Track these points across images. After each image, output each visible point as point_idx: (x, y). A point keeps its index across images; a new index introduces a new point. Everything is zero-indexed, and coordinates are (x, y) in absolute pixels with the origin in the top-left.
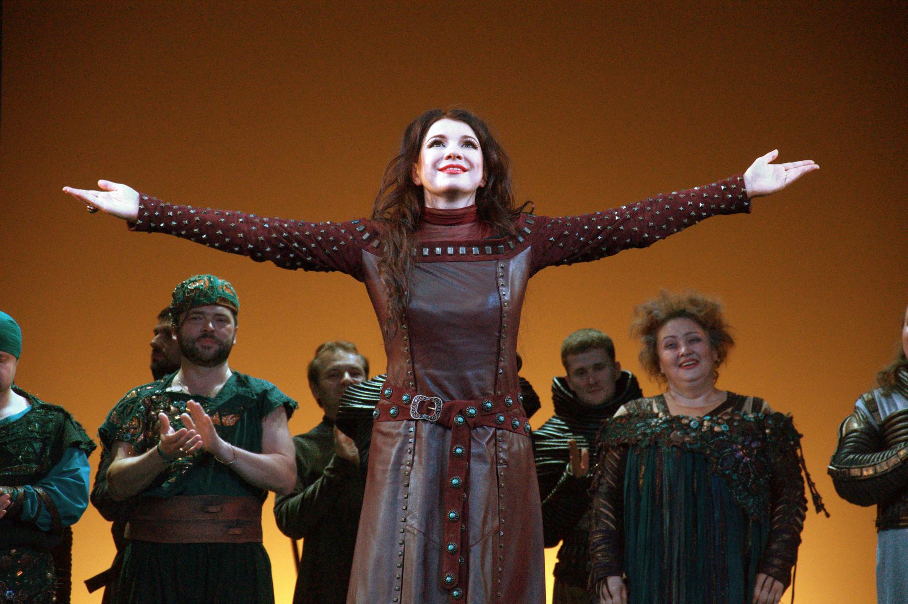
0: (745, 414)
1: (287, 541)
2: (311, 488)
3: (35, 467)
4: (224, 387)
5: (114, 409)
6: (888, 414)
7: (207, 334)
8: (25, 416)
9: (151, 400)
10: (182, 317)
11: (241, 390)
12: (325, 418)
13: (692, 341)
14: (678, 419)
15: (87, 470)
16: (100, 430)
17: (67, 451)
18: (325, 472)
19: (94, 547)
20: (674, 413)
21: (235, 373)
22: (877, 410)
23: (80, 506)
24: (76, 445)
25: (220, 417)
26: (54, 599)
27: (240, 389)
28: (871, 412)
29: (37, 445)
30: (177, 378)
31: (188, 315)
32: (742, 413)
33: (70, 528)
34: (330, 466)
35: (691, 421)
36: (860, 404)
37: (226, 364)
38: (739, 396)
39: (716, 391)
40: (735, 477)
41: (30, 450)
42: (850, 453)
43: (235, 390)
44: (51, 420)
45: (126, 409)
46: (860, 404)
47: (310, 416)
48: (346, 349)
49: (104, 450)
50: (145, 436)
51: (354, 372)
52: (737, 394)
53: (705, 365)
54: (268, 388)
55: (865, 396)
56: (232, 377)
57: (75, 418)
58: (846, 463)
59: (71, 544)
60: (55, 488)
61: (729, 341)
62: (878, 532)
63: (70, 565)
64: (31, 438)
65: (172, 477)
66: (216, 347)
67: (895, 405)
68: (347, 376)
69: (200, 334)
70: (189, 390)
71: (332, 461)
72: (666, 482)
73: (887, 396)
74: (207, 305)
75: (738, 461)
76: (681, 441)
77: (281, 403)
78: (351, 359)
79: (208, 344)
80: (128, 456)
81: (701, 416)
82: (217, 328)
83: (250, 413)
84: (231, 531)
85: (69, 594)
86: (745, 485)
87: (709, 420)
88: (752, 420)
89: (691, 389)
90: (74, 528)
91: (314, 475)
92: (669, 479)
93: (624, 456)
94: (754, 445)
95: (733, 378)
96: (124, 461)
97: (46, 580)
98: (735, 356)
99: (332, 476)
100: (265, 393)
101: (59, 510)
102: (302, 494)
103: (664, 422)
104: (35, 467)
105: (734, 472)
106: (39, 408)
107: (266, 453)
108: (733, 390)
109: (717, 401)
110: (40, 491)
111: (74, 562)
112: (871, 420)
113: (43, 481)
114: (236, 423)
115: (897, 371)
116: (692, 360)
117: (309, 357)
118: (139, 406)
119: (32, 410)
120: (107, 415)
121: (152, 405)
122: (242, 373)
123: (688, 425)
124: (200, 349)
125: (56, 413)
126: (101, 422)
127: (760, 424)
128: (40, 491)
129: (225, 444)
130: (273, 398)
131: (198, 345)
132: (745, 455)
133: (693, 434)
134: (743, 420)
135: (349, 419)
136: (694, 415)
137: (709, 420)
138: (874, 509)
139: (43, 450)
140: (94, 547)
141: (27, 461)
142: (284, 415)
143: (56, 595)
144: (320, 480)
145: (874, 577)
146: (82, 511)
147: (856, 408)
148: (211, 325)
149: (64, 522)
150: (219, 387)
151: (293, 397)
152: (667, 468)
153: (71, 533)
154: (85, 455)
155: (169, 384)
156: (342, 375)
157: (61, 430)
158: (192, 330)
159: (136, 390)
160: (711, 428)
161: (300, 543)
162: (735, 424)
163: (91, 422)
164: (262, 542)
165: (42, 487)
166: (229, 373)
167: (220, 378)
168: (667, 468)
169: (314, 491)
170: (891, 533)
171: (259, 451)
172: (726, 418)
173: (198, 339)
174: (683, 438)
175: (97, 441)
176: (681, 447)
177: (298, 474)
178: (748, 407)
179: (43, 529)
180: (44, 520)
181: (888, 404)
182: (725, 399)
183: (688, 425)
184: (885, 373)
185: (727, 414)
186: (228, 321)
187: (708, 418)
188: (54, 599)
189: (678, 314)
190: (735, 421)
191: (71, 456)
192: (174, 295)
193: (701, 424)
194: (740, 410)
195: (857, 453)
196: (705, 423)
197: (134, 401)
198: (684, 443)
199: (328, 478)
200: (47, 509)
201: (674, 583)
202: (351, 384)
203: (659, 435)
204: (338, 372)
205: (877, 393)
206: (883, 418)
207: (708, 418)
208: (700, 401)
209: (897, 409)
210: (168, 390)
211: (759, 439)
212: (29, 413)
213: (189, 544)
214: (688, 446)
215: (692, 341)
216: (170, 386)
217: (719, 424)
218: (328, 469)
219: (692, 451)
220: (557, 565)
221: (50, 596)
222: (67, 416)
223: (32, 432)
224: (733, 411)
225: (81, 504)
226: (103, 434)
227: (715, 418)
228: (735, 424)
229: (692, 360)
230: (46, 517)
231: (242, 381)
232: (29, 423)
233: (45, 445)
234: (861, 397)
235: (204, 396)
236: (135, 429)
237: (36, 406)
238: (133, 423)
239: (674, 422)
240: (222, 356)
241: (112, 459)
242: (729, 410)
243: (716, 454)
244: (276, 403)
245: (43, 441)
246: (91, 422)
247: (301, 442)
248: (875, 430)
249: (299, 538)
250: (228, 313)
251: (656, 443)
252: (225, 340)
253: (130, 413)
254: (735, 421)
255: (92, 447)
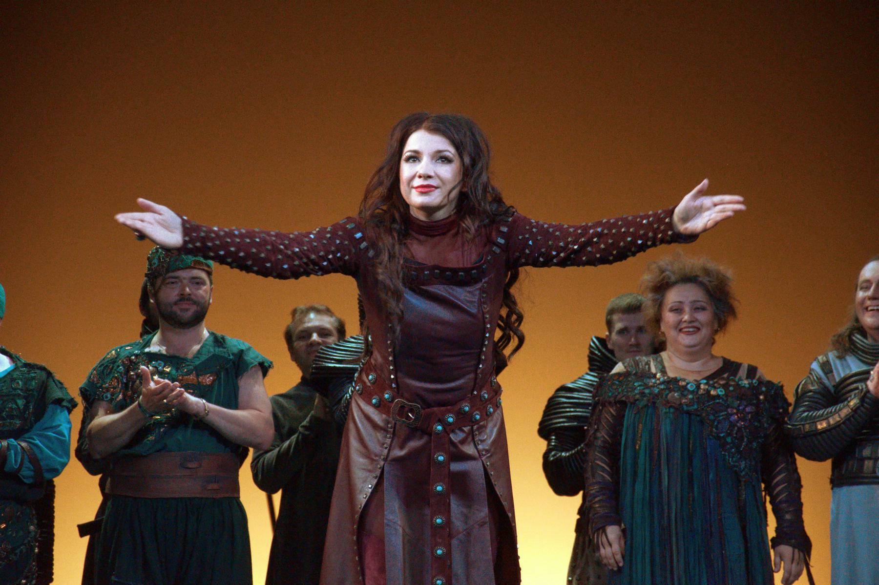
0: (740, 380)
1: (263, 495)
2: (287, 443)
3: (18, 423)
4: (202, 347)
5: (94, 369)
6: (842, 375)
7: (183, 298)
8: (9, 374)
9: (131, 361)
10: (159, 282)
11: (218, 350)
12: (303, 378)
13: (697, 309)
14: (676, 380)
15: (69, 424)
16: (81, 389)
17: (50, 408)
18: (300, 429)
19: (78, 498)
20: (671, 374)
21: (212, 334)
22: (832, 371)
23: (62, 460)
24: (59, 402)
25: (197, 376)
26: (36, 550)
27: (217, 349)
28: (826, 374)
29: (21, 402)
30: (156, 338)
31: (164, 279)
32: (737, 379)
33: (53, 482)
34: (304, 423)
35: (688, 384)
36: (815, 366)
37: (204, 323)
38: (733, 362)
39: (713, 357)
40: (729, 440)
41: (14, 406)
42: (804, 412)
43: (212, 350)
44: (33, 378)
45: (106, 368)
46: (815, 366)
47: (286, 377)
48: (318, 311)
49: (85, 408)
50: (124, 395)
51: (323, 332)
52: (732, 360)
53: (705, 332)
54: (244, 348)
55: (820, 358)
56: (209, 337)
57: (57, 377)
58: (802, 420)
59: (53, 497)
60: (37, 442)
61: (731, 311)
62: (832, 489)
63: (53, 517)
64: (15, 395)
65: (151, 434)
66: (193, 309)
67: (849, 366)
68: (315, 337)
69: (177, 298)
70: (166, 351)
71: (308, 419)
72: (664, 441)
73: (841, 358)
74: (182, 269)
75: (732, 425)
76: (678, 402)
77: (256, 363)
78: (326, 322)
79: (185, 306)
80: (107, 414)
81: (698, 379)
82: (194, 291)
83: (227, 373)
84: (210, 487)
85: (52, 545)
86: (738, 447)
87: (706, 384)
88: (747, 386)
89: (689, 354)
90: (57, 481)
91: (292, 432)
92: (667, 438)
93: (619, 419)
94: (748, 409)
95: (728, 346)
96: (103, 419)
97: (29, 532)
98: (733, 326)
99: (307, 433)
100: (241, 352)
101: (42, 463)
102: (278, 449)
103: (661, 384)
104: (18, 423)
105: (729, 435)
106: (22, 367)
107: (243, 409)
108: (728, 357)
109: (714, 366)
110: (23, 444)
111: (57, 514)
112: (826, 382)
113: (26, 435)
114: (214, 381)
115: (850, 335)
116: (694, 327)
117: (287, 321)
118: (118, 366)
119: (16, 369)
120: (88, 374)
121: (131, 364)
122: (219, 334)
123: (685, 387)
124: (179, 312)
125: (38, 371)
126: (82, 382)
127: (755, 390)
128: (23, 444)
129: (193, 399)
130: (249, 357)
131: (175, 308)
132: (740, 419)
133: (690, 396)
134: (738, 385)
135: (322, 381)
136: (691, 378)
137: (706, 384)
138: (828, 463)
139: (26, 406)
140: (78, 498)
141: (12, 417)
142: (260, 374)
143: (38, 547)
144: (296, 436)
145: (828, 533)
146: (64, 465)
147: (812, 370)
148: (188, 289)
149: (47, 476)
150: (197, 347)
151: (268, 357)
152: (666, 428)
153: (54, 486)
154: (66, 412)
155: (147, 344)
156: (310, 336)
157: (43, 388)
158: (170, 294)
159: (116, 351)
160: (708, 392)
161: (277, 497)
162: (731, 388)
163: (73, 380)
164: (238, 498)
165: (26, 441)
166: (206, 333)
167: (198, 339)
168: (666, 428)
169: (290, 446)
170: (845, 490)
171: (236, 407)
172: (722, 382)
173: (176, 303)
174: (680, 399)
175: (79, 400)
176: (678, 409)
177: (276, 430)
178: (743, 372)
179: (26, 481)
180: (27, 473)
181: (842, 365)
182: (721, 365)
183: (685, 387)
184: (840, 336)
185: (723, 379)
186: (204, 283)
187: (705, 381)
188: (36, 550)
189: (688, 279)
190: (730, 385)
191: (54, 413)
192: (148, 258)
193: (698, 387)
194: (735, 376)
195: (809, 411)
196: (702, 386)
197: (113, 361)
198: (681, 404)
199: (303, 435)
200: (30, 462)
201: (674, 539)
202: (319, 344)
203: (657, 395)
204: (308, 333)
205: (832, 356)
206: (837, 380)
207: (705, 381)
208: (696, 365)
209: (850, 369)
210: (147, 350)
211: (753, 405)
212: (13, 371)
213: (168, 499)
214: (685, 408)
215: (697, 309)
216: (149, 346)
217: (715, 388)
218: (303, 427)
219: (688, 413)
220: (578, 521)
221: (32, 549)
222: (49, 374)
223: (15, 389)
224: (728, 378)
225: (61, 457)
226: (84, 392)
227: (711, 382)
228: (731, 388)
229: (694, 327)
230: (29, 469)
231: (219, 341)
232: (13, 380)
233: (28, 402)
234: (816, 359)
235: (182, 356)
236: (114, 388)
237: (20, 364)
238: (114, 381)
239: (672, 383)
240: (198, 318)
241: (92, 418)
242: (725, 376)
243: (712, 417)
244: (252, 363)
245: (25, 398)
246: (73, 380)
247: (278, 402)
248: (829, 391)
249: (276, 491)
250: (203, 275)
251: (654, 403)
252: (203, 301)
253: (110, 372)
254: (730, 385)
255: (75, 405)
